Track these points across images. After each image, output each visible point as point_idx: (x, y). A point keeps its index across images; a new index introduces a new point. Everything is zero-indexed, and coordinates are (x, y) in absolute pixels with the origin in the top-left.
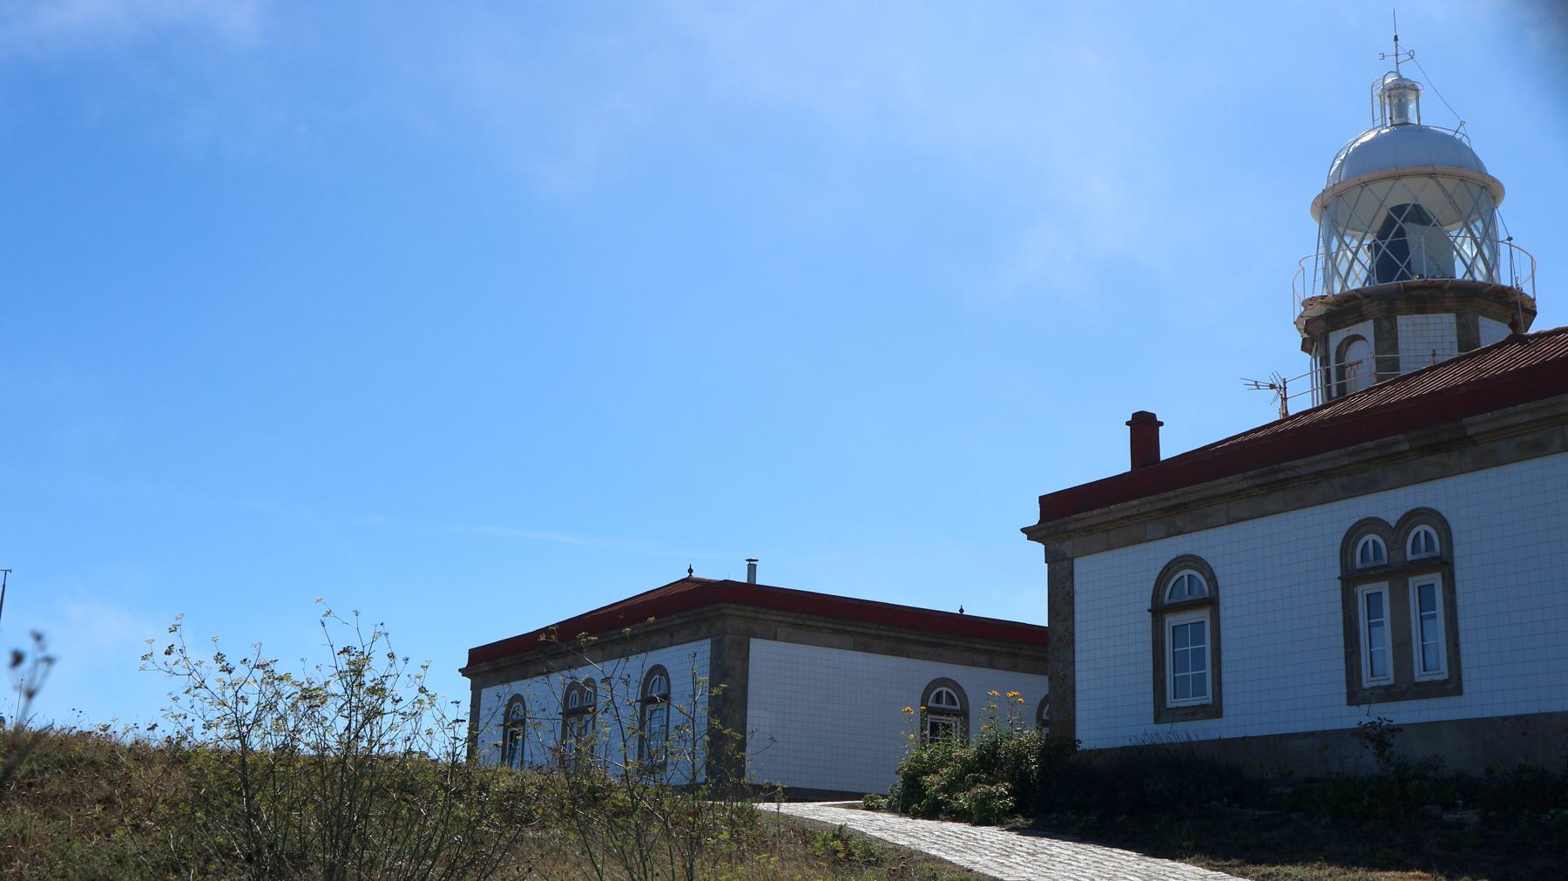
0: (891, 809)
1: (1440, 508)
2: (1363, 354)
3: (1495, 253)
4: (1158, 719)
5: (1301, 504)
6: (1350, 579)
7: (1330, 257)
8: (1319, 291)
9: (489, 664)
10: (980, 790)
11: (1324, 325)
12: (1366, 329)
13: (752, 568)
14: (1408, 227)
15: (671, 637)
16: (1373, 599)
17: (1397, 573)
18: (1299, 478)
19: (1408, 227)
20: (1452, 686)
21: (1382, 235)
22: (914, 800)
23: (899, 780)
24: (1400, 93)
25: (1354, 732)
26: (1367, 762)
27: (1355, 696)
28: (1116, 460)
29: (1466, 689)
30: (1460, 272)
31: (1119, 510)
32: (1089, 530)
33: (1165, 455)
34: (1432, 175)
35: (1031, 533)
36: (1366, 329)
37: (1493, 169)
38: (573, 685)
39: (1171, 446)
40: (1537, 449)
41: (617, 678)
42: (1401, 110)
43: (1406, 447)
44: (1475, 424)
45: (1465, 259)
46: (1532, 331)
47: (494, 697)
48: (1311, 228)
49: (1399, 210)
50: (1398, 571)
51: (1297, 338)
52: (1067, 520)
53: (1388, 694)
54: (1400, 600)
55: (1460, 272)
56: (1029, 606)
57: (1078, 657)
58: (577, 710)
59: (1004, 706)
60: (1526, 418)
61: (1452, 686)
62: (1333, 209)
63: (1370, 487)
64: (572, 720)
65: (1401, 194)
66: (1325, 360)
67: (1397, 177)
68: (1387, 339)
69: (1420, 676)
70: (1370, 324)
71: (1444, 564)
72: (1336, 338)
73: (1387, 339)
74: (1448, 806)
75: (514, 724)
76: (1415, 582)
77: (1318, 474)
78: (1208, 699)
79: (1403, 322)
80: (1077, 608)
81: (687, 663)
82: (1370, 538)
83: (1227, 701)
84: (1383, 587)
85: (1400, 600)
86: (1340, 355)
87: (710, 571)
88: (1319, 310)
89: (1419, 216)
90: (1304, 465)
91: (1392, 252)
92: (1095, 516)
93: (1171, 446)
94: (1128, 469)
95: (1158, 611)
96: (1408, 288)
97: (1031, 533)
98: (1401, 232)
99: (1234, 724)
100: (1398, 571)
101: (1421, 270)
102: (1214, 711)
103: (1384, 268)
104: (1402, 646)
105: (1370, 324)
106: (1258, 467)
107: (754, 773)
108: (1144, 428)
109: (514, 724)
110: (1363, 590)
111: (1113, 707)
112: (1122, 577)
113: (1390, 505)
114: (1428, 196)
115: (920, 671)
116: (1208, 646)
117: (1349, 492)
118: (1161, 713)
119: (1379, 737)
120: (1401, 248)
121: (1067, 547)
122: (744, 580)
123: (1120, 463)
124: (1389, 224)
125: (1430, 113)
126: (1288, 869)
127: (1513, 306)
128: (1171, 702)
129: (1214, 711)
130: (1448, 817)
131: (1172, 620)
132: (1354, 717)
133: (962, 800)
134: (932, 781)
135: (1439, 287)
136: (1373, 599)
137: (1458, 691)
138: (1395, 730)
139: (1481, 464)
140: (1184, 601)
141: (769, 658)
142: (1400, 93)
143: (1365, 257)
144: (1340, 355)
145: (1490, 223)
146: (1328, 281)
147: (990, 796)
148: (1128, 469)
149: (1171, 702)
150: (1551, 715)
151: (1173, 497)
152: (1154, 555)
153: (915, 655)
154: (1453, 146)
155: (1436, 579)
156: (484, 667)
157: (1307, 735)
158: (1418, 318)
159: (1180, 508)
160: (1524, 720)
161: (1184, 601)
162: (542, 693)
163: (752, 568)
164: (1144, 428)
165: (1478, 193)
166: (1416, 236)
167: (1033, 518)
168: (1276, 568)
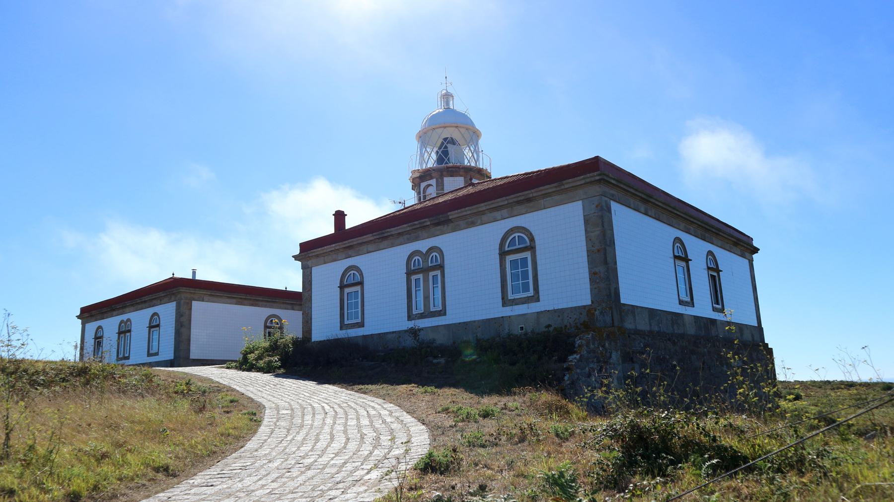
0: (236, 368)
1: (440, 246)
2: (432, 191)
3: (478, 156)
4: (341, 328)
5: (392, 246)
6: (409, 273)
7: (422, 155)
8: (418, 167)
9: (89, 313)
10: (267, 359)
11: (420, 179)
12: (433, 182)
13: (194, 273)
14: (448, 145)
15: (161, 301)
16: (417, 280)
17: (425, 271)
18: (392, 235)
19: (448, 145)
20: (442, 313)
21: (440, 148)
22: (245, 365)
23: (242, 356)
24: (447, 97)
25: (406, 331)
26: (409, 342)
27: (410, 318)
28: (329, 229)
29: (541, 298)
30: (466, 162)
31: (327, 248)
32: (317, 256)
33: (348, 226)
34: (457, 127)
35: (296, 258)
36: (433, 182)
37: (478, 126)
38: (122, 322)
39: (349, 224)
40: (473, 224)
41: (139, 318)
42: (447, 103)
43: (428, 223)
44: (453, 215)
45: (468, 160)
46: (614, 206)
47: (92, 327)
48: (415, 145)
49: (445, 139)
50: (426, 269)
51: (410, 184)
52: (310, 252)
53: (422, 316)
54: (426, 281)
55: (466, 162)
56: (295, 284)
57: (313, 305)
58: (124, 331)
59: (291, 325)
60: (469, 212)
61: (442, 313)
62: (423, 138)
63: (417, 239)
64: (122, 335)
65: (447, 134)
66: (419, 193)
67: (445, 127)
68: (440, 185)
69: (432, 309)
70: (434, 180)
71: (441, 267)
72: (423, 185)
73: (440, 185)
74: (436, 357)
75: (98, 340)
76: (431, 274)
77: (399, 234)
78: (359, 320)
79: (446, 179)
80: (313, 287)
81: (167, 311)
82: (417, 258)
83: (366, 321)
84: (420, 276)
85: (426, 281)
86: (424, 191)
87: (178, 275)
88: (417, 175)
89: (453, 142)
90: (394, 231)
91: (443, 156)
92: (319, 251)
93: (349, 224)
94: (333, 232)
95: (342, 287)
96: (448, 168)
97: (296, 258)
98: (446, 147)
99: (369, 329)
100: (426, 269)
101: (453, 161)
102: (361, 325)
103: (440, 160)
104: (426, 298)
105: (434, 180)
106: (380, 231)
107: (194, 355)
108: (340, 217)
109: (98, 340)
110: (414, 277)
111: (325, 326)
112: (329, 274)
113: (423, 245)
114: (455, 134)
115: (261, 313)
116: (359, 300)
117: (410, 241)
118: (343, 326)
119: (414, 332)
120: (446, 153)
121: (309, 263)
122: (190, 277)
123: (329, 229)
124: (442, 144)
125: (458, 105)
126: (366, 386)
127: (481, 173)
128: (511, 296)
129: (361, 325)
130: (435, 361)
131: (347, 290)
132: (407, 325)
133: (261, 363)
134: (251, 357)
135: (458, 167)
136: (417, 280)
137: (445, 314)
138: (420, 330)
139: (454, 230)
140: (351, 283)
141: (203, 311)
142: (447, 97)
143: (434, 156)
144: (424, 191)
145: (476, 145)
146: (421, 164)
147: (270, 362)
148: (333, 232)
149: (511, 296)
150: (474, 321)
151: (347, 243)
152: (342, 265)
153: (265, 306)
154: (464, 116)
155: (438, 273)
156: (86, 315)
157: (393, 332)
158: (451, 179)
159: (350, 247)
160: (466, 324)
161: (351, 283)
162: (110, 325)
163: (194, 273)
164: (340, 217)
165: (474, 135)
166: (451, 148)
167: (297, 251)
168: (384, 268)
